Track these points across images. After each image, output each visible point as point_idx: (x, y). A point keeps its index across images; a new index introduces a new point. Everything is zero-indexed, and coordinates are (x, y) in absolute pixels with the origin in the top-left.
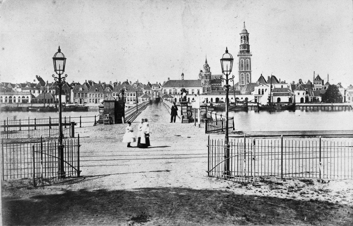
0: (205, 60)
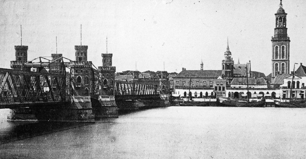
0: (227, 46)
